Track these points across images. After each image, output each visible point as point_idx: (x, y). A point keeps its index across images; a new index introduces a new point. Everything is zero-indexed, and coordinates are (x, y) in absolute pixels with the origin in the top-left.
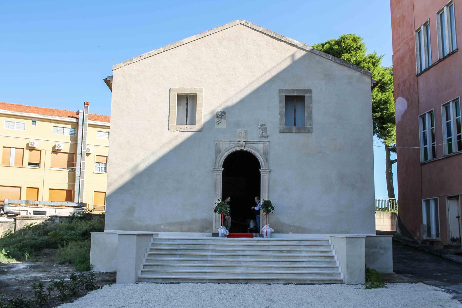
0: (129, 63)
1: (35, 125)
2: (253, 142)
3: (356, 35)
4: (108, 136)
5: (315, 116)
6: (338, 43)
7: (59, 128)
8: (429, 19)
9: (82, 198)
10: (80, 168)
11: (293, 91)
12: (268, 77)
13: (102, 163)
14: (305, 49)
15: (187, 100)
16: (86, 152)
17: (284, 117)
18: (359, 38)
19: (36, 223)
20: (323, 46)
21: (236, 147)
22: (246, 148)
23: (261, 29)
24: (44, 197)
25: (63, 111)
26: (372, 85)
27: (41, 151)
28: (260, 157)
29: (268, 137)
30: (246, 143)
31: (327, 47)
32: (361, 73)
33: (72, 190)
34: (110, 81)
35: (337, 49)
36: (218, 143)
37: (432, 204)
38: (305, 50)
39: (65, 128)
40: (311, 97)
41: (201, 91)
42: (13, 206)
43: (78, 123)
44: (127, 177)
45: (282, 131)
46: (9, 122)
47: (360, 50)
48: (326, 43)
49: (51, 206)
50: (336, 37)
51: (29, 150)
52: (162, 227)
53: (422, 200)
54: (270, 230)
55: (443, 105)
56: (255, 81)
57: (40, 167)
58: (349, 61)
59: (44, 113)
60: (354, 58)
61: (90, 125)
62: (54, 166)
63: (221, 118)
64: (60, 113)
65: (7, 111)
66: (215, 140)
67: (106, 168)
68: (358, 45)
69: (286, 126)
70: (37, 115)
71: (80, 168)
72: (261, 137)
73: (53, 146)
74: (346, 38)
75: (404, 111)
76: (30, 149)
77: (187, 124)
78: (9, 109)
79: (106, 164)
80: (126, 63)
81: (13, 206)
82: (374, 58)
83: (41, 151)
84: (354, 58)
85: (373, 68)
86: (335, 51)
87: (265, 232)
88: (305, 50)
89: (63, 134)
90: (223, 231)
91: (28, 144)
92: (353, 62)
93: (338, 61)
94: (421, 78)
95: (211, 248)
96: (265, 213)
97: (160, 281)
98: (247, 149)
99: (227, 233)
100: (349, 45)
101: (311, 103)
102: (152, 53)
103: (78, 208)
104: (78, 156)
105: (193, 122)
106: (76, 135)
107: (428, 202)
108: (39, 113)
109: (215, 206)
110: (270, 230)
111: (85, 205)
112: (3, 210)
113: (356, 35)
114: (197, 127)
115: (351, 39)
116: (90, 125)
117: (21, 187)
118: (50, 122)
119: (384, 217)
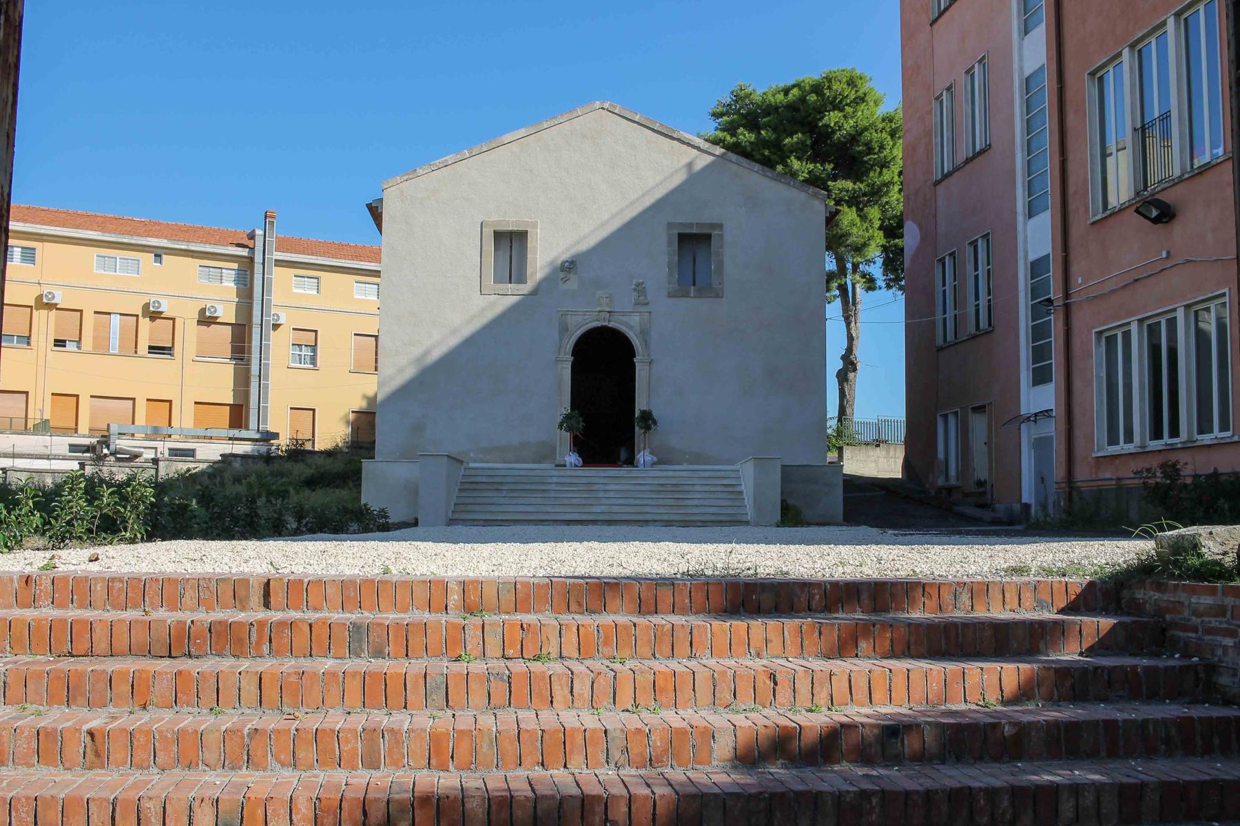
0: (411, 176)
1: (159, 264)
2: (624, 314)
3: (856, 72)
4: (318, 286)
5: (730, 268)
6: (817, 89)
7: (211, 269)
8: (988, 52)
9: (265, 422)
10: (261, 357)
11: (691, 225)
12: (648, 201)
13: (306, 346)
14: (713, 152)
15: (511, 242)
16: (272, 322)
17: (676, 270)
18: (861, 78)
19: (196, 468)
20: (786, 92)
21: (594, 321)
22: (610, 323)
23: (637, 118)
24: (185, 418)
25: (215, 231)
26: (828, 215)
27: (173, 319)
28: (635, 337)
29: (648, 304)
30: (611, 314)
31: (794, 96)
32: (808, 194)
33: (242, 405)
34: (377, 207)
35: (815, 102)
36: (565, 314)
37: (952, 421)
38: (713, 155)
39: (224, 271)
40: (721, 236)
41: (535, 225)
42: (128, 438)
43: (251, 260)
44: (410, 373)
45: (670, 295)
46: (104, 257)
47: (865, 104)
48: (794, 86)
49: (205, 437)
50: (812, 75)
51: (148, 319)
52: (472, 455)
53: (938, 415)
54: (650, 458)
55: (970, 244)
56: (627, 207)
57: (173, 356)
58: (839, 127)
59: (176, 235)
60: (851, 122)
61: (279, 263)
62: (203, 353)
63: (570, 273)
64: (209, 236)
65: (100, 233)
66: (559, 309)
67: (314, 355)
68: (860, 94)
69: (679, 285)
70: (165, 241)
71: (261, 357)
72: (636, 304)
73: (144, 305)
74: (833, 79)
75: (914, 249)
76: (150, 317)
77: (511, 283)
78: (103, 230)
79: (314, 348)
80: (405, 178)
81: (128, 438)
82: (894, 121)
83: (173, 319)
84: (851, 122)
85: (891, 143)
86: (811, 107)
87: (642, 462)
88: (713, 155)
89: (221, 283)
90: (572, 458)
91: (146, 306)
92: (848, 129)
93: (770, 174)
94: (940, 188)
95: (555, 480)
96: (643, 431)
97: (482, 523)
98: (612, 325)
99: (579, 462)
100: (840, 94)
101: (722, 246)
102: (450, 159)
103: (261, 443)
104: (256, 331)
105: (522, 280)
106: (248, 286)
107: (945, 417)
108: (169, 240)
109: (559, 419)
110: (650, 458)
111: (276, 436)
112: (108, 447)
113: (856, 72)
114: (526, 288)
115: (844, 80)
116: (279, 263)
117: (134, 399)
118: (192, 257)
119: (895, 455)
